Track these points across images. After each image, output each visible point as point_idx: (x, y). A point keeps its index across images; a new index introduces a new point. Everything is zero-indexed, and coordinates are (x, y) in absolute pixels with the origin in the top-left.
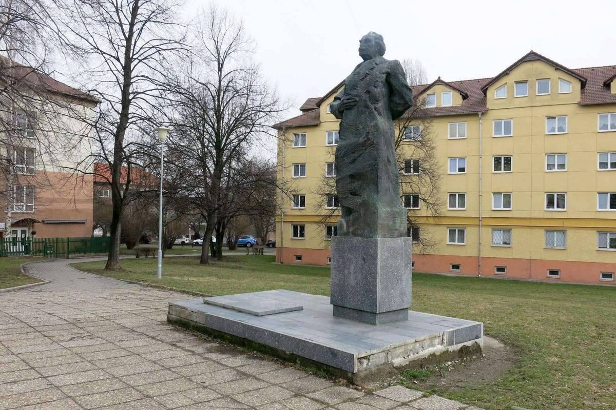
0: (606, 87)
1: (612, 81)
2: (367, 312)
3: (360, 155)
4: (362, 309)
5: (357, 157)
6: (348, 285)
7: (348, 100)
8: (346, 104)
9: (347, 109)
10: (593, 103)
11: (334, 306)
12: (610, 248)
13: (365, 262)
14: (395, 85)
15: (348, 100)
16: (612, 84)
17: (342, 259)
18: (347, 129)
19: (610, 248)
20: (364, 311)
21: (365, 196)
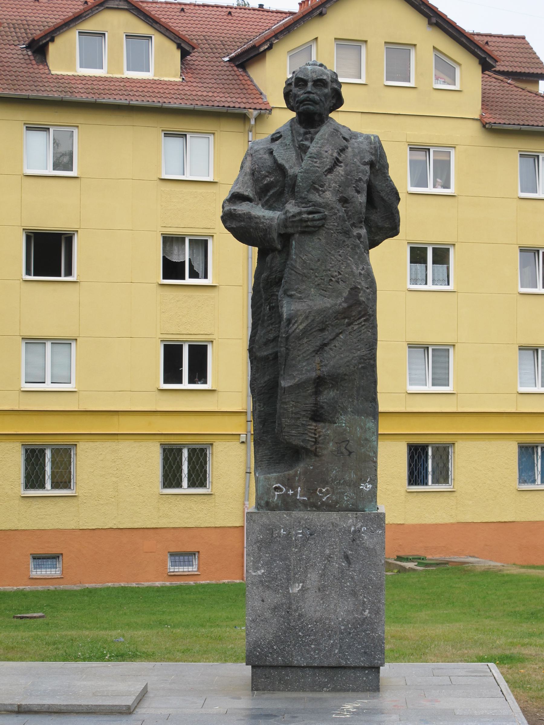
0: (34, 52)
1: (52, 40)
2: (355, 668)
3: (338, 335)
4: (343, 663)
5: (331, 340)
6: (300, 616)
7: (310, 213)
8: (306, 221)
9: (303, 233)
10: (12, 93)
11: (253, 667)
12: (189, 487)
13: (349, 563)
14: (379, 188)
15: (310, 213)
16: (52, 48)
17: (281, 560)
18: (304, 275)
19: (189, 487)
20: (350, 668)
21: (343, 421)
